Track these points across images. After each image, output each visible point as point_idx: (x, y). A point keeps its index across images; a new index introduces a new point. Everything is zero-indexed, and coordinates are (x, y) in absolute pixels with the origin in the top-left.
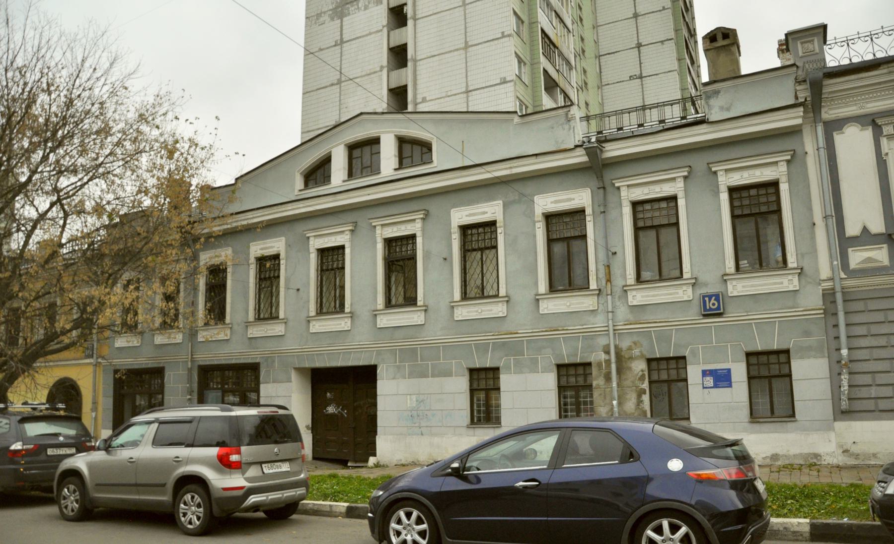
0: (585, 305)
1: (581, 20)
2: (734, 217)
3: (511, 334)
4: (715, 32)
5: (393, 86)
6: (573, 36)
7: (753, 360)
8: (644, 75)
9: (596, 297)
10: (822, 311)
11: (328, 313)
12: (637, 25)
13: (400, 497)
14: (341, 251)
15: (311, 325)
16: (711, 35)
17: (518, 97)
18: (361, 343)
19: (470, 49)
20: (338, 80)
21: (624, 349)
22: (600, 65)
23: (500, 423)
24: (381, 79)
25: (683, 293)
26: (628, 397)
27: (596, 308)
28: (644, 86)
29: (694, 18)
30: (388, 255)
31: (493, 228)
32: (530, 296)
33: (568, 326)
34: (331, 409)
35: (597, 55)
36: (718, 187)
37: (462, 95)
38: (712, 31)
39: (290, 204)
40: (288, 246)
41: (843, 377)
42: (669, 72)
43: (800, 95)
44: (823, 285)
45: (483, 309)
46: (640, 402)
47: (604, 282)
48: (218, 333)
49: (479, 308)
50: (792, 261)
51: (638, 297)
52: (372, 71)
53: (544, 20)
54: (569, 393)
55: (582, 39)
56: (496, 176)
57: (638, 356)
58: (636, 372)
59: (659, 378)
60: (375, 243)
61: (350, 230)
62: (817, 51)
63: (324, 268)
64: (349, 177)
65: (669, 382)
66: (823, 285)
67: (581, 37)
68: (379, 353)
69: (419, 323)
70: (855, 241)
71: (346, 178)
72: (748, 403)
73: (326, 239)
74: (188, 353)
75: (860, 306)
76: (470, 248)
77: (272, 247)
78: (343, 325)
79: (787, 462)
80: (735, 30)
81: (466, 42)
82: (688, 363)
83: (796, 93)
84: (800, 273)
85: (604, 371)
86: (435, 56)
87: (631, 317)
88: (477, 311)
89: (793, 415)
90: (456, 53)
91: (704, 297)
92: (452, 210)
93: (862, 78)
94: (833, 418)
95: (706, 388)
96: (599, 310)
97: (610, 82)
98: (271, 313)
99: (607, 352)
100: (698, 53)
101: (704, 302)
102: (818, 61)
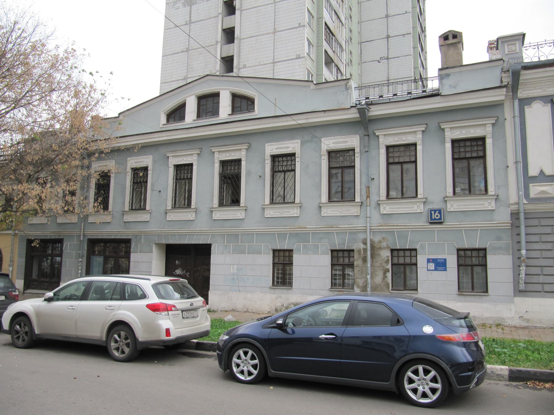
0: (352, 212)
1: (351, 17)
2: (454, 159)
3: (302, 228)
4: (448, 33)
5: (224, 56)
6: (345, 28)
7: (462, 253)
8: (389, 57)
9: (359, 207)
10: (510, 225)
11: (179, 208)
12: (387, 23)
13: (240, 341)
14: (190, 167)
16: (445, 35)
17: (307, 68)
19: (277, 34)
20: (187, 48)
21: (376, 242)
22: (361, 49)
23: (292, 286)
24: (216, 51)
25: (416, 207)
26: (378, 273)
27: (359, 214)
28: (389, 65)
29: (425, 19)
30: (222, 172)
31: (293, 158)
33: (340, 225)
35: (360, 42)
36: (444, 138)
37: (269, 65)
38: (445, 33)
39: (156, 134)
40: (154, 161)
41: (521, 268)
42: (407, 56)
43: (503, 80)
44: (511, 207)
45: (101, 217)
46: (385, 277)
47: (365, 197)
48: (104, 217)
50: (491, 190)
51: (386, 209)
52: (211, 44)
53: (327, 17)
54: (337, 268)
55: (351, 31)
56: (299, 123)
57: (385, 247)
58: (383, 257)
59: (398, 262)
60: (214, 163)
61: (197, 154)
62: (518, 51)
63: (178, 178)
64: (197, 118)
65: (405, 265)
66: (511, 207)
67: (350, 29)
69: (192, 219)
70: (534, 179)
71: (195, 118)
72: (457, 282)
74: (81, 230)
75: (535, 222)
76: (277, 170)
78: (190, 216)
80: (462, 33)
81: (275, 29)
82: (418, 253)
83: (501, 79)
84: (496, 198)
85: (362, 256)
86: (253, 37)
88: (338, 211)
89: (487, 291)
90: (267, 36)
91: (431, 211)
92: (266, 144)
93: (547, 71)
94: (513, 295)
95: (429, 270)
96: (361, 216)
97: (367, 61)
98: (140, 206)
99: (365, 244)
100: (426, 44)
101: (431, 214)
102: (519, 58)
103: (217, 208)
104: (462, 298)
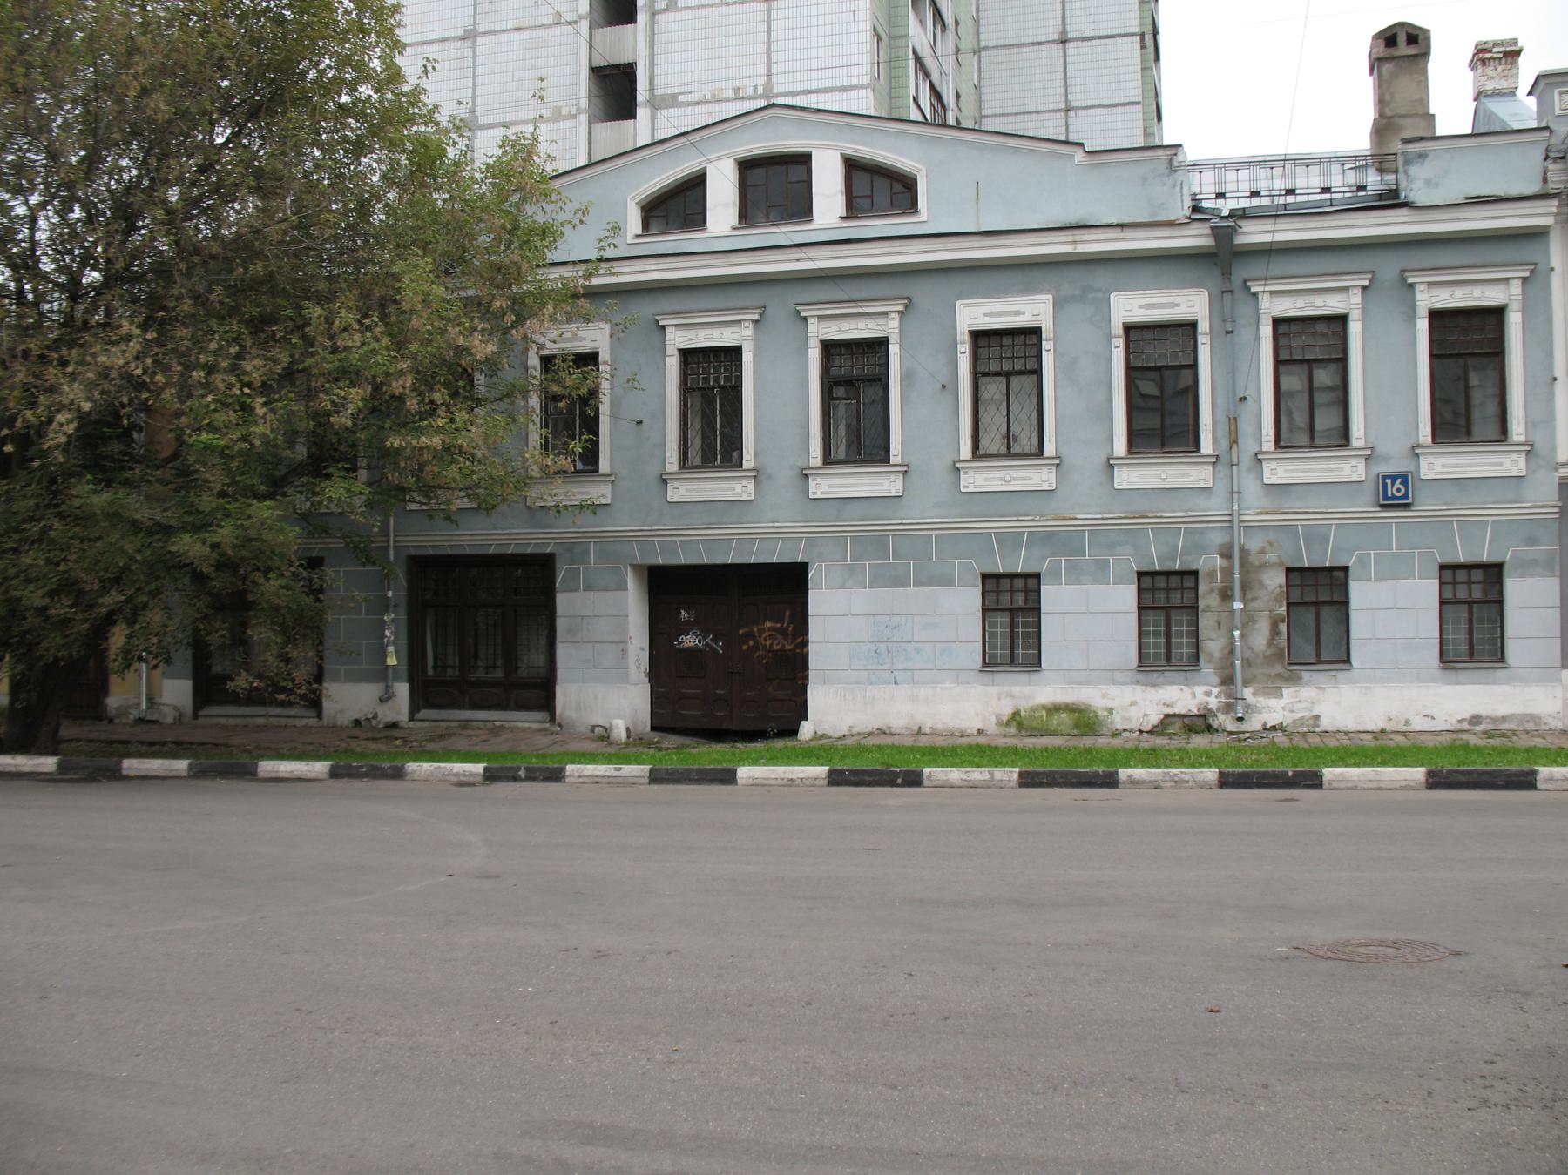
0: (1191, 479)
7: (1147, 581)
10: (1556, 510)
15: (670, 487)
18: (777, 524)
27: (1211, 485)
29: (1158, 33)
32: (1100, 458)
34: (689, 640)
36: (1413, 307)
43: (1551, 177)
44: (1561, 471)
47: (1224, 444)
49: (1007, 475)
50: (1049, 449)
51: (1279, 471)
61: (752, 320)
68: (811, 543)
69: (745, 497)
73: (701, 333)
77: (1018, 313)
79: (1491, 727)
83: (1545, 174)
87: (1265, 503)
88: (1001, 479)
101: (1385, 486)
103: (675, 473)
104: (1451, 674)
